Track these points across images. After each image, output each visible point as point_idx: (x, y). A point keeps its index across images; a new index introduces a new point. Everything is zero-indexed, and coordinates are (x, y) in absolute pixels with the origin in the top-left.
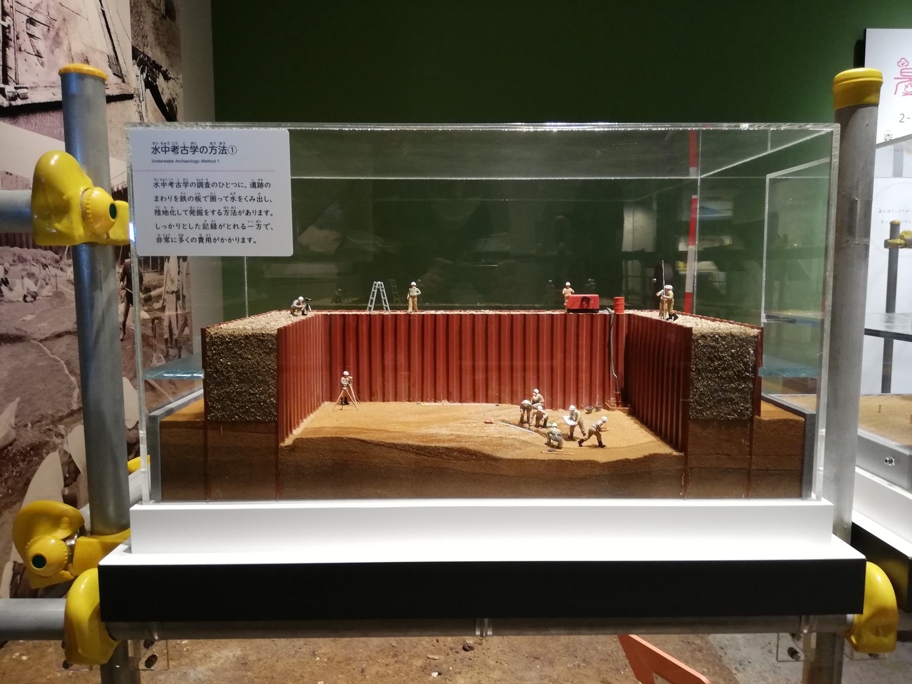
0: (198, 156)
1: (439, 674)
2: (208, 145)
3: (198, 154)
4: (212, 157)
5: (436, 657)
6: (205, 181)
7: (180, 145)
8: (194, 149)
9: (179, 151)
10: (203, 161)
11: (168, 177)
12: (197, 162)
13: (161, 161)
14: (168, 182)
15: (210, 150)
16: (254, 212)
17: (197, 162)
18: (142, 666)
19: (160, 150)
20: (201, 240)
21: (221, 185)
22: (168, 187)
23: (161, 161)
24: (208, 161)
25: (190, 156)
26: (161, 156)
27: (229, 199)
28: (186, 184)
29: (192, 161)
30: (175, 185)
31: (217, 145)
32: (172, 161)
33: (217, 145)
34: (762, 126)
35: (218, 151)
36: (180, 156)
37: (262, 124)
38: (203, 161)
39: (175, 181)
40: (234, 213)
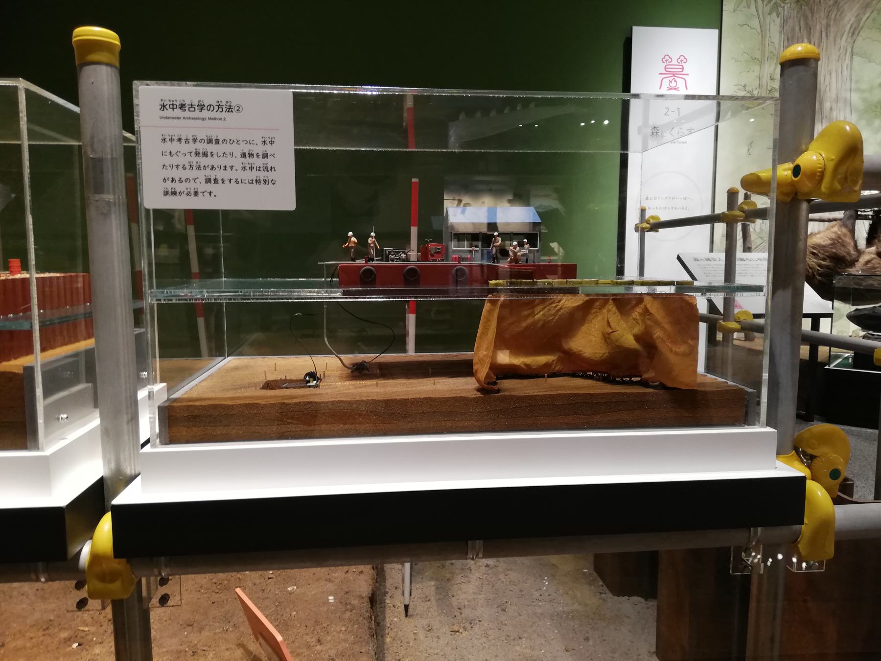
0: (205, 114)
1: (79, 645)
2: (215, 104)
3: (205, 112)
4: (218, 115)
5: (86, 629)
6: (214, 138)
7: (188, 102)
8: (201, 107)
9: (187, 108)
10: (210, 119)
11: (176, 133)
12: (204, 119)
13: (169, 118)
14: (176, 138)
15: (216, 108)
16: (219, 167)
17: (204, 119)
18: (155, 601)
19: (167, 107)
20: (196, 193)
21: (232, 142)
22: (176, 143)
23: (169, 118)
24: (215, 119)
25: (197, 114)
26: (169, 113)
27: (193, 154)
28: (195, 140)
29: (199, 118)
30: (183, 141)
31: (224, 103)
32: (180, 118)
33: (224, 103)
34: (396, 90)
35: (224, 109)
36: (187, 114)
37: (176, 82)
38: (210, 119)
39: (183, 138)
40: (199, 168)
